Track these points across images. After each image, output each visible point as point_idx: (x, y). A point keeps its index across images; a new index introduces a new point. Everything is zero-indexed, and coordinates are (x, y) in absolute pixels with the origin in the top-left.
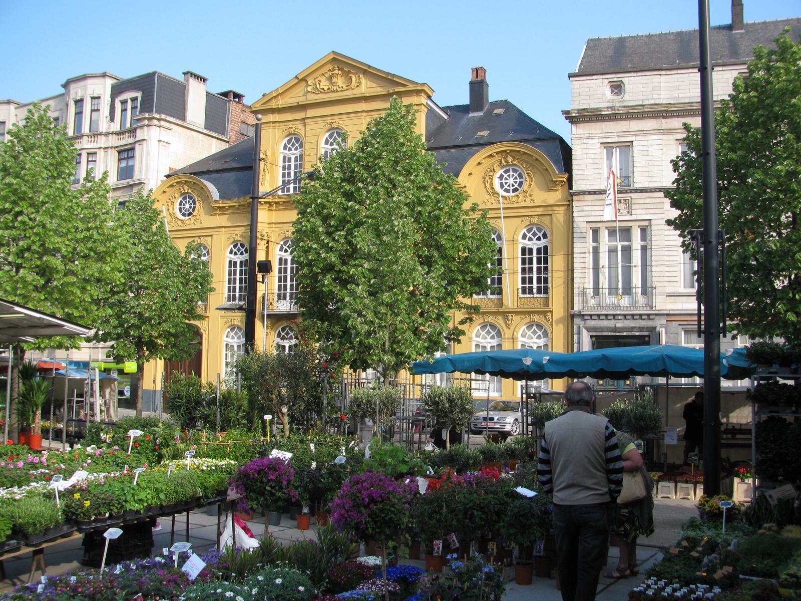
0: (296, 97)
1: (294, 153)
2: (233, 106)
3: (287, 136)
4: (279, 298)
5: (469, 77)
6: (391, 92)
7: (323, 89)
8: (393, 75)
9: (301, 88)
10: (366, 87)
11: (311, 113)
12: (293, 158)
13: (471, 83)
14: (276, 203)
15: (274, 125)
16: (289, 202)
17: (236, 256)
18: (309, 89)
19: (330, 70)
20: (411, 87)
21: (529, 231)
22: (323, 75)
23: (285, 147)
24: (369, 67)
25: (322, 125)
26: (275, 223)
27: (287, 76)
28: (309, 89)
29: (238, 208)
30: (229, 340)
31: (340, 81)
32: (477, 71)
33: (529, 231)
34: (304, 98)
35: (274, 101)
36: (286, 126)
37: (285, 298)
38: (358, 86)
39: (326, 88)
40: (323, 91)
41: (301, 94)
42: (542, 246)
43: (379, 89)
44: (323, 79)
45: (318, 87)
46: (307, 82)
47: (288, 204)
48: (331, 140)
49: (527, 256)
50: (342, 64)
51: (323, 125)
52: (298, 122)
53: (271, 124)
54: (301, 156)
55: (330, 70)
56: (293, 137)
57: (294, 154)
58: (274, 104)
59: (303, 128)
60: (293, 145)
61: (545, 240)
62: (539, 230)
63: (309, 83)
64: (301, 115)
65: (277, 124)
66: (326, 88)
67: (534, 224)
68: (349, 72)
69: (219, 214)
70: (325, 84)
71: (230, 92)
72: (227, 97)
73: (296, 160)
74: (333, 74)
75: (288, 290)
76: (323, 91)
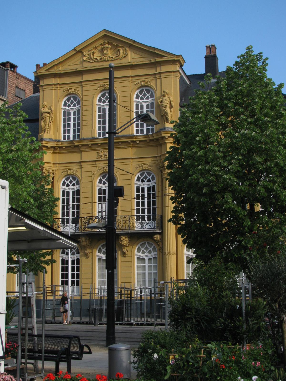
0: (74, 65)
1: (73, 108)
2: (10, 74)
3: (101, 92)
4: (63, 223)
5: (204, 53)
6: (152, 61)
7: (96, 59)
8: (155, 49)
9: (78, 58)
10: (131, 57)
11: (86, 77)
12: (145, 105)
13: (206, 57)
14: (60, 147)
15: (56, 86)
16: (70, 147)
17: (144, 183)
18: (85, 58)
19: (101, 45)
20: (169, 58)
21: (67, 179)
22: (96, 48)
23: (65, 104)
24: (134, 42)
25: (96, 87)
26: (59, 164)
27: (66, 48)
28: (85, 58)
29: (148, 142)
30: (140, 254)
31: (110, 53)
32: (211, 49)
33: (67, 179)
34: (80, 66)
35: (55, 68)
36: (67, 87)
37: (68, 223)
38: (125, 57)
39: (99, 58)
40: (96, 61)
41: (78, 62)
42: (76, 190)
43: (142, 60)
44: (96, 51)
45: (92, 57)
46: (83, 53)
47: (70, 148)
48: (141, 96)
49: (151, 193)
50: (110, 40)
51: (97, 86)
52: (150, 77)
53: (54, 86)
54: (79, 111)
55: (101, 45)
56: (72, 96)
57: (72, 109)
58: (56, 70)
59: (80, 89)
60: (72, 102)
61: (78, 186)
62: (74, 179)
63: (85, 54)
64: (78, 79)
65: (58, 86)
66: (99, 58)
67: (145, 170)
68: (117, 46)
69: (59, 153)
70: (97, 55)
71: (8, 63)
72: (5, 67)
73: (74, 114)
74: (104, 47)
75: (146, 213)
76: (96, 61)
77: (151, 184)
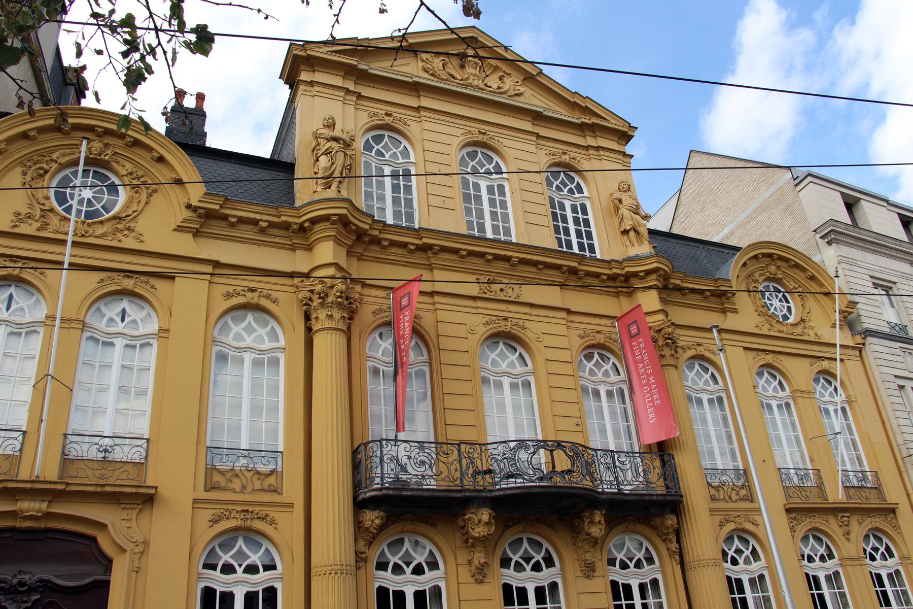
24: (368, 39)
77: (648, 573)
